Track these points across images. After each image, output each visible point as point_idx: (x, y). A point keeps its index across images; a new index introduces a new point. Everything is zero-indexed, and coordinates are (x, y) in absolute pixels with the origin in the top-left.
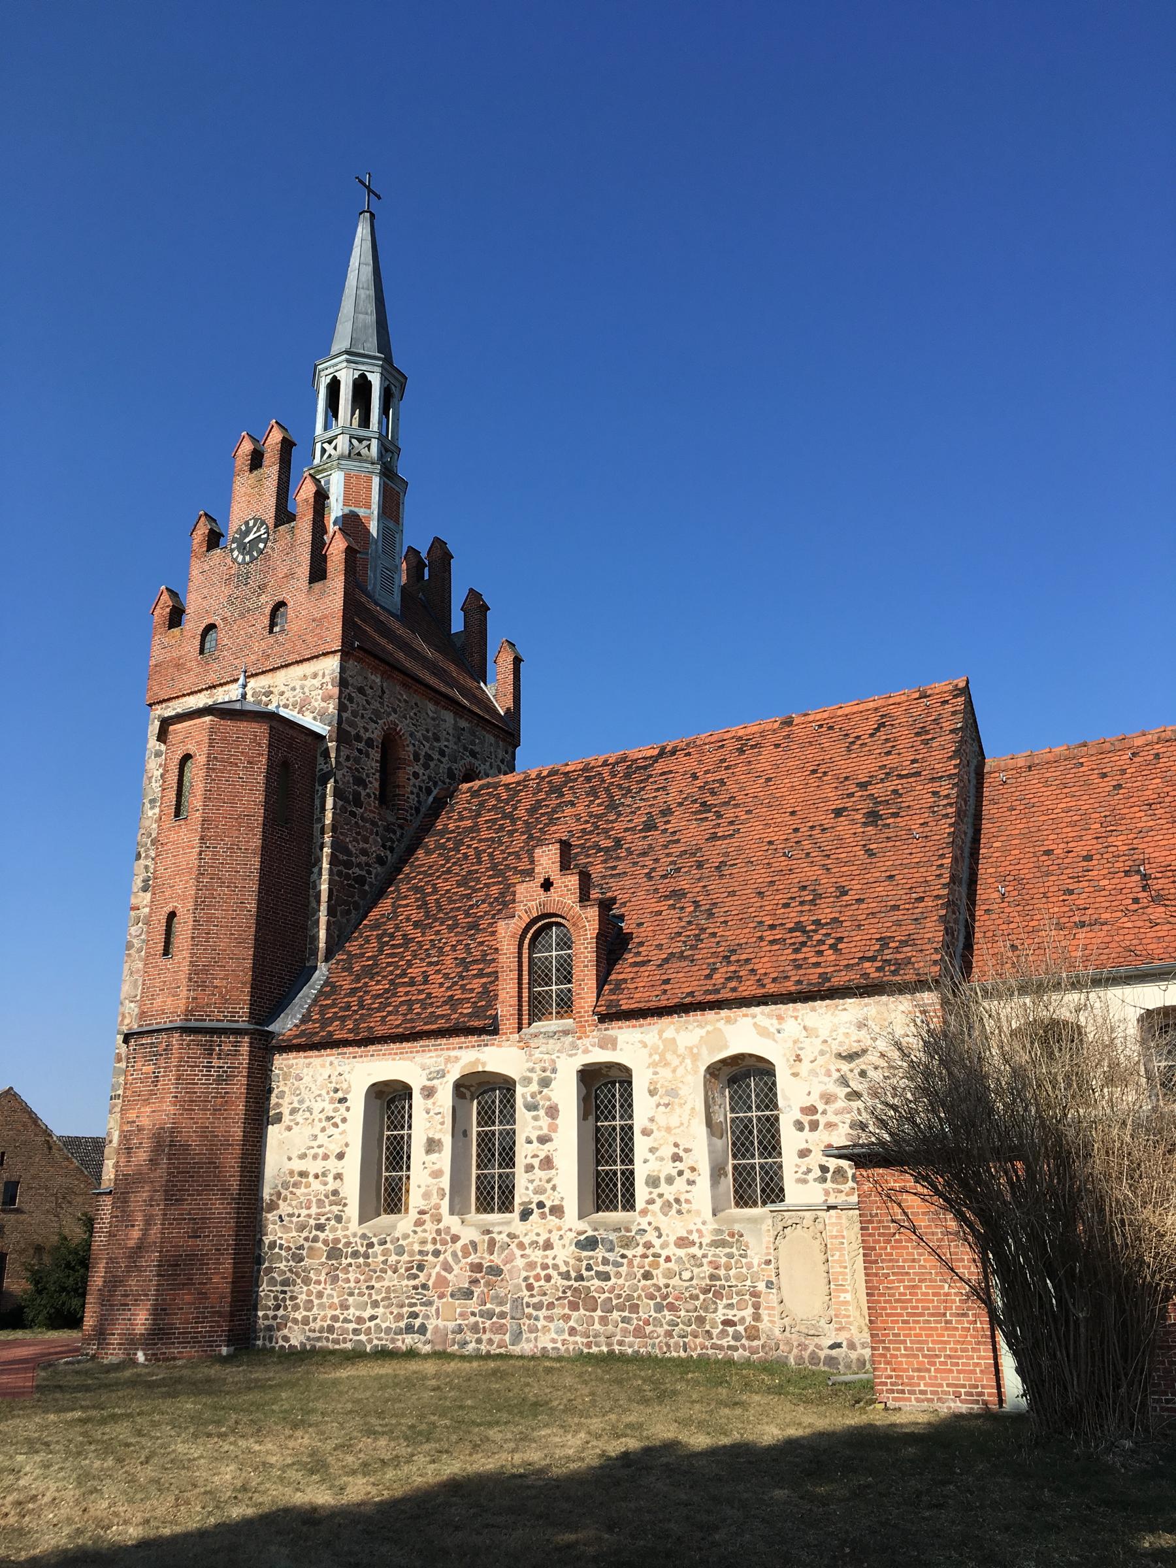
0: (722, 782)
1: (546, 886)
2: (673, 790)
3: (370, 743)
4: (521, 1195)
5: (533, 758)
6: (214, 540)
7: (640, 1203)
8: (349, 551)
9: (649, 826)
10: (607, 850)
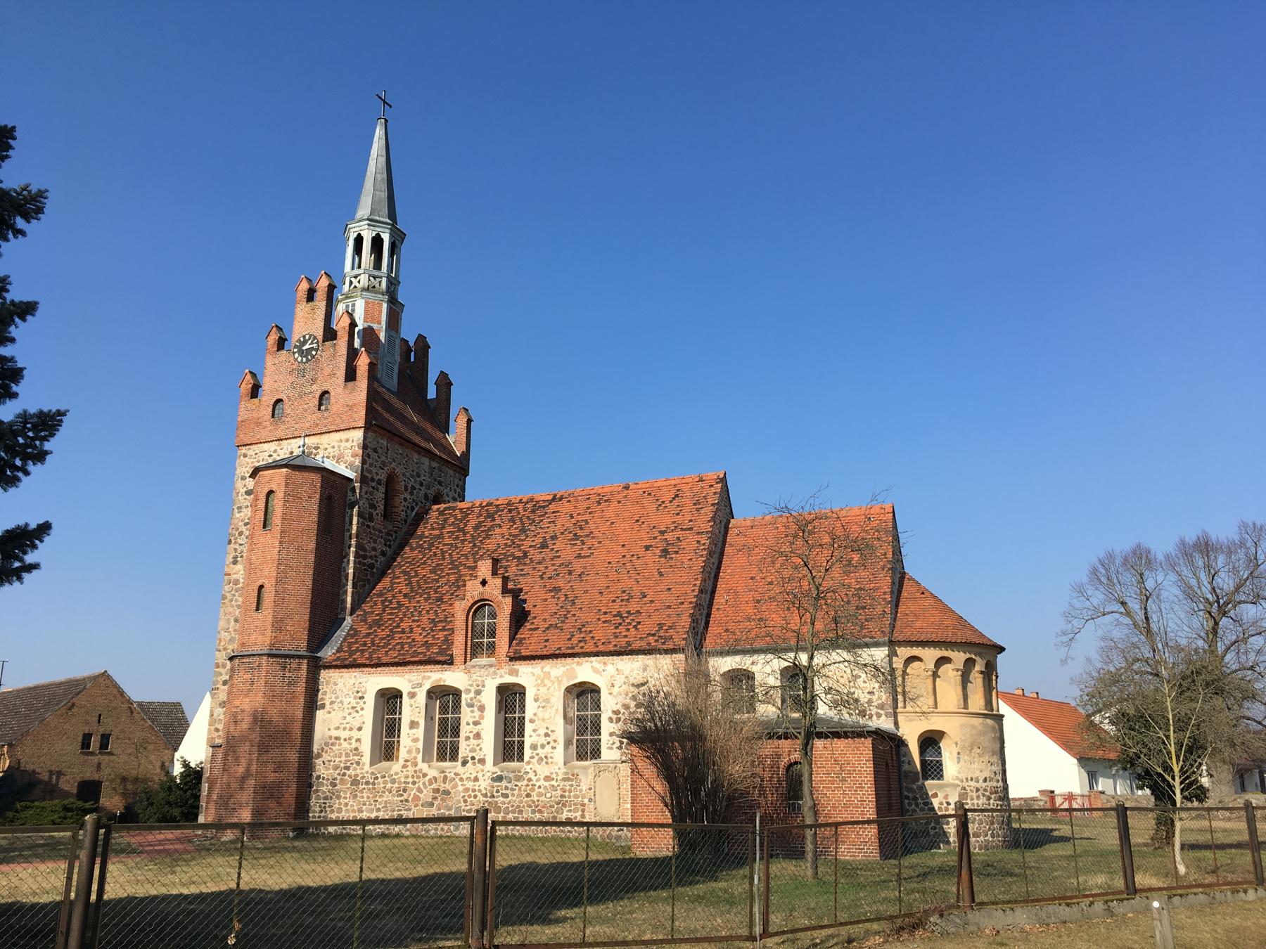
0: (587, 522)
1: (482, 583)
2: (559, 523)
3: (379, 482)
4: (464, 750)
5: (478, 490)
6: (281, 344)
7: (526, 758)
8: (372, 366)
9: (544, 546)
10: (519, 558)
